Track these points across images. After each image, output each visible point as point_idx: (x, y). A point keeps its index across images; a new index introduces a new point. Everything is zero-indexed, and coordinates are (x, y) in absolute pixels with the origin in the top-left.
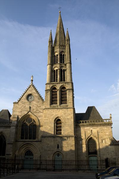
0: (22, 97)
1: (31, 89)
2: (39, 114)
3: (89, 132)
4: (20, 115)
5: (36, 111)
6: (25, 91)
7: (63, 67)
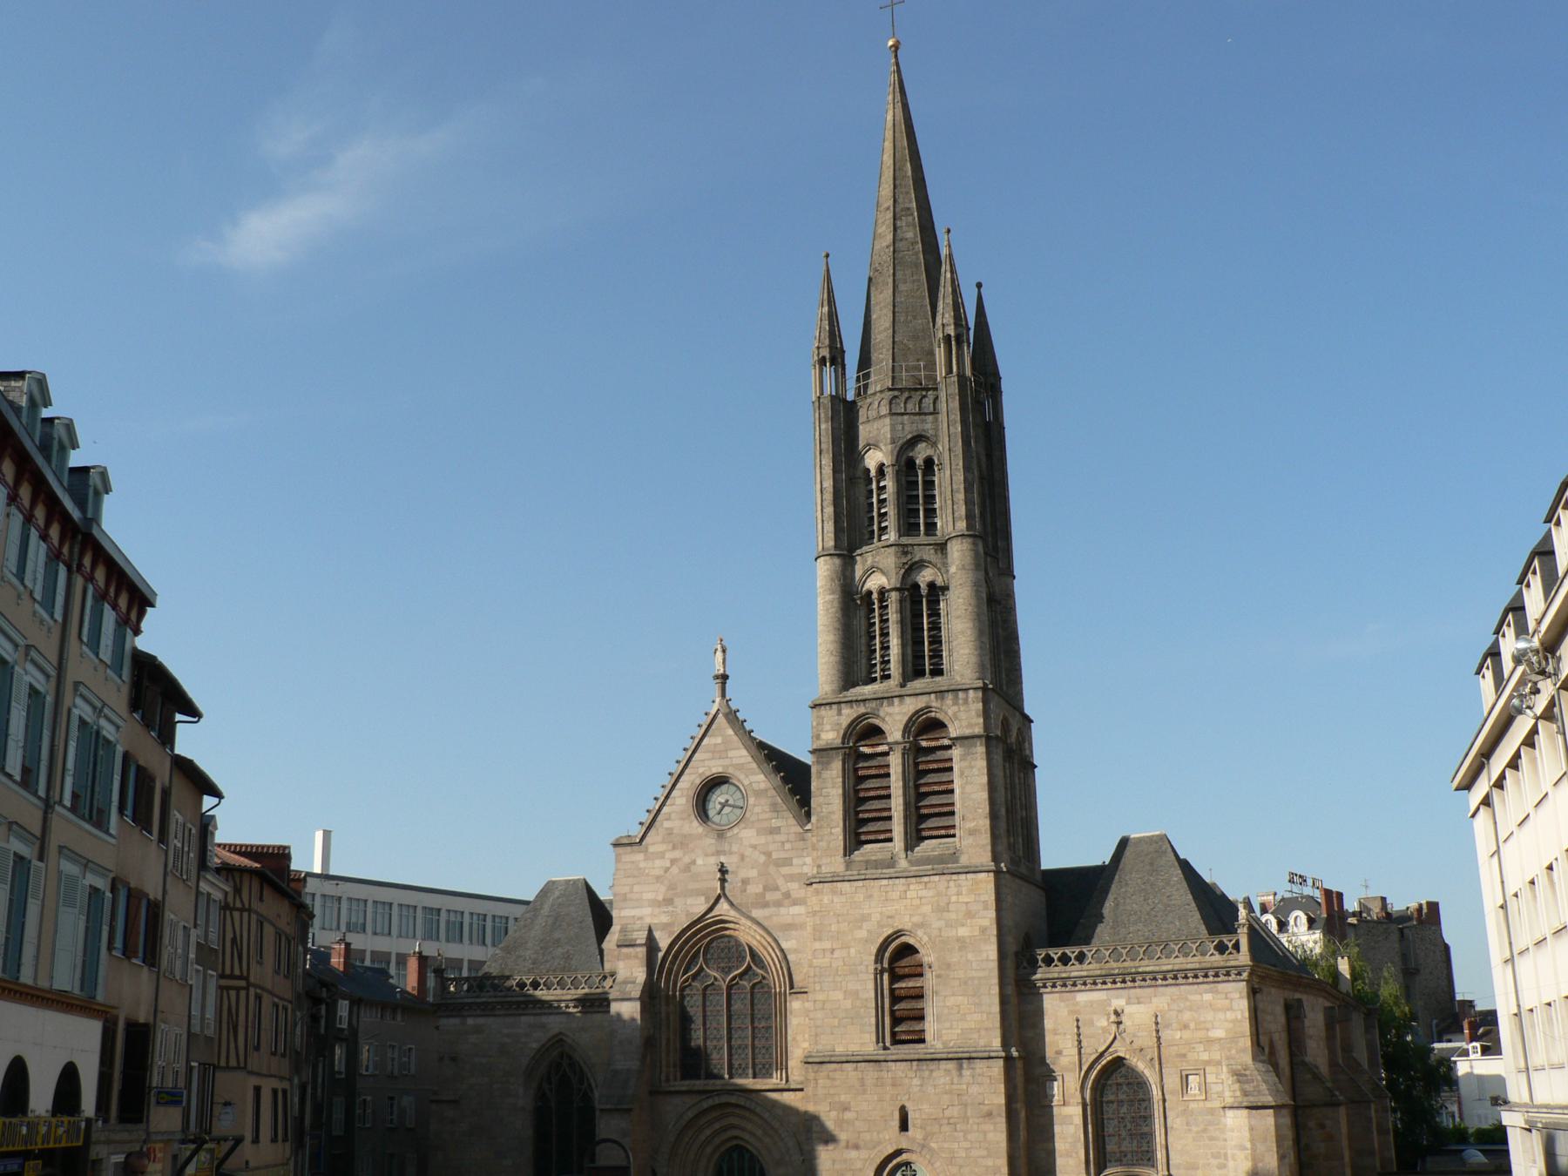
0: (667, 797)
1: (719, 740)
2: (783, 910)
3: (1104, 1023)
4: (665, 927)
6: (684, 757)
7: (919, 565)
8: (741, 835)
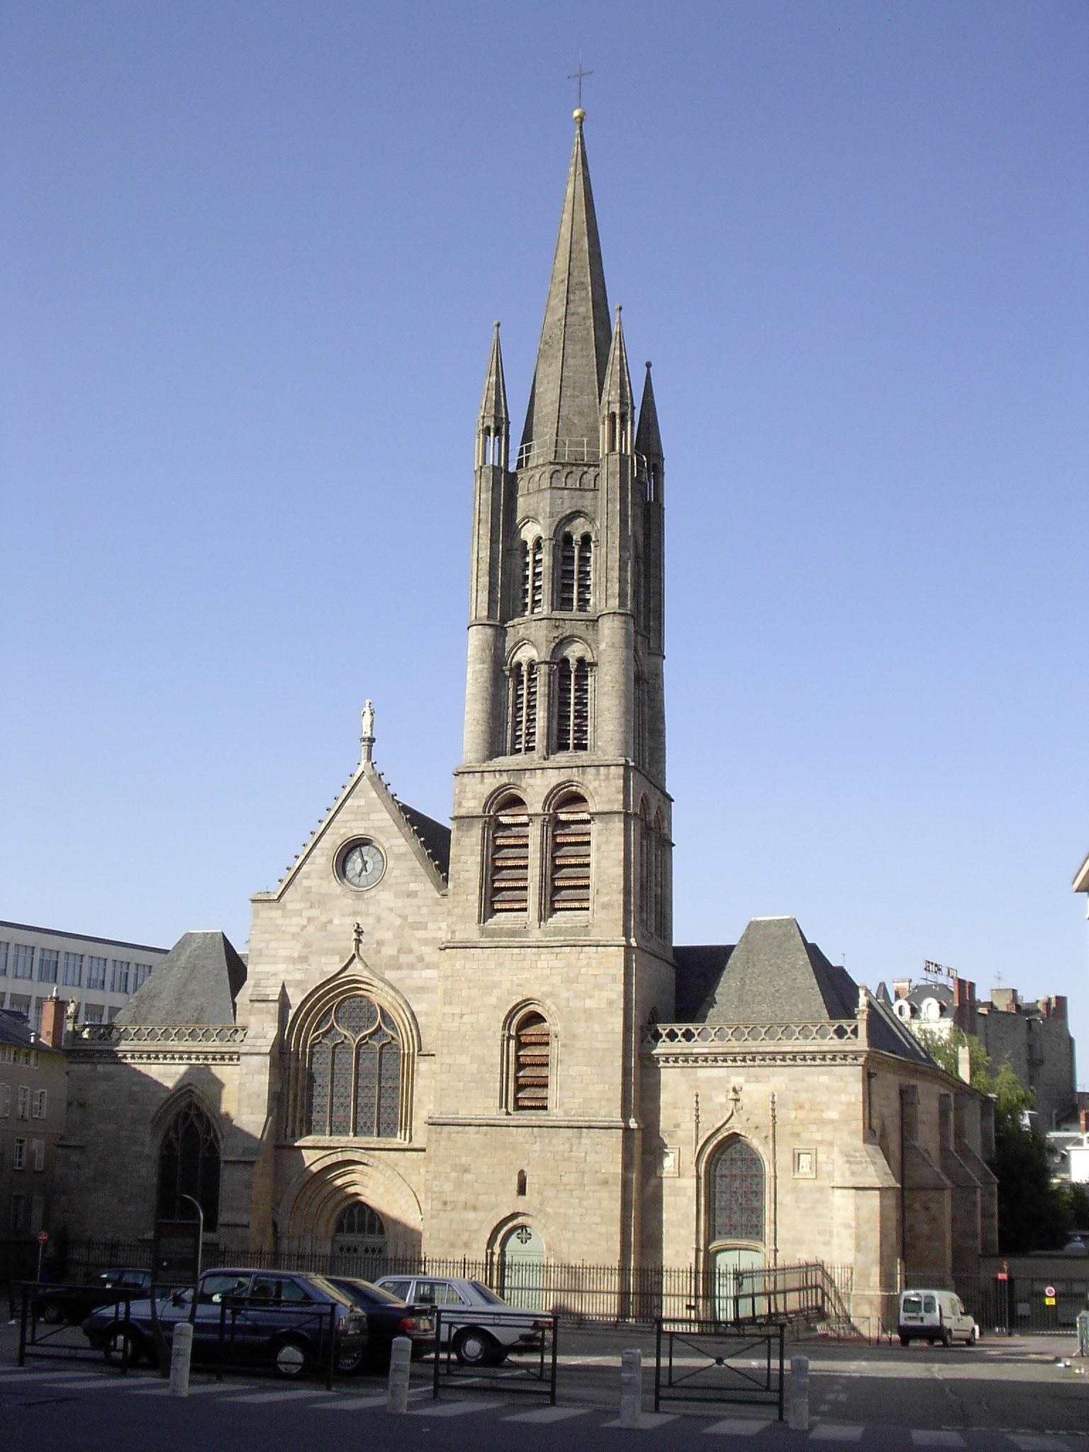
1: (362, 802)
2: (415, 973)
3: (722, 1099)
4: (299, 983)
5: (397, 958)
8: (378, 897)
